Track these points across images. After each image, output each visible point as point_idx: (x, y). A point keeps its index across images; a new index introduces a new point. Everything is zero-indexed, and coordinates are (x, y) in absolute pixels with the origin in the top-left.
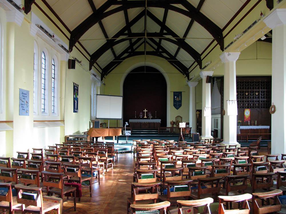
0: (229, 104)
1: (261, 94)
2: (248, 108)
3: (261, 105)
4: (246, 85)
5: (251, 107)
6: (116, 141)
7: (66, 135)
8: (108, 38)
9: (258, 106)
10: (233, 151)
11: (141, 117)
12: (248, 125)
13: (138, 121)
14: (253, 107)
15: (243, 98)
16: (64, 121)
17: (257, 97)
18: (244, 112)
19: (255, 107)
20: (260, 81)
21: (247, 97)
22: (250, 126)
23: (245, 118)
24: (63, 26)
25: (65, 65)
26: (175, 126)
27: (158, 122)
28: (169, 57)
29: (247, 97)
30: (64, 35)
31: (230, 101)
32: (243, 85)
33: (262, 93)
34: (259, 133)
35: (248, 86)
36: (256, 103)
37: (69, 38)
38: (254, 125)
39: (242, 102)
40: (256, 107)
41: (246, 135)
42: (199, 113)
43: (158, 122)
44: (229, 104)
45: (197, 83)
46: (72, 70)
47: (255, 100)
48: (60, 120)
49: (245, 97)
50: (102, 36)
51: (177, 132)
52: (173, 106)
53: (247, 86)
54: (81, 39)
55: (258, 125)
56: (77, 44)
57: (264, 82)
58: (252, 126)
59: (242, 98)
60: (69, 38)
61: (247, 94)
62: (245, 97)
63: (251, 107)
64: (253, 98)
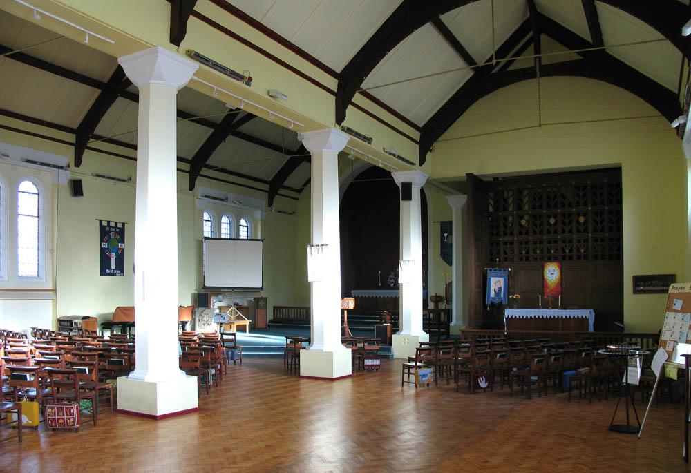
1: (562, 221)
2: (550, 259)
5: (564, 258)
7: (58, 317)
8: (476, 64)
9: (526, 255)
11: (392, 285)
12: (538, 307)
13: (376, 293)
14: (571, 258)
15: (541, 233)
16: (54, 290)
17: (582, 228)
20: (589, 182)
22: (543, 308)
23: (548, 287)
25: (66, 191)
26: (442, 306)
36: (505, 246)
38: (555, 307)
39: (538, 245)
40: (579, 258)
41: (485, 334)
46: (79, 199)
47: (575, 236)
48: (51, 288)
49: (502, 233)
50: (460, 63)
51: (299, 317)
52: (440, 257)
55: (564, 307)
57: (585, 188)
58: (548, 308)
61: (552, 221)
62: (502, 233)
63: (564, 258)
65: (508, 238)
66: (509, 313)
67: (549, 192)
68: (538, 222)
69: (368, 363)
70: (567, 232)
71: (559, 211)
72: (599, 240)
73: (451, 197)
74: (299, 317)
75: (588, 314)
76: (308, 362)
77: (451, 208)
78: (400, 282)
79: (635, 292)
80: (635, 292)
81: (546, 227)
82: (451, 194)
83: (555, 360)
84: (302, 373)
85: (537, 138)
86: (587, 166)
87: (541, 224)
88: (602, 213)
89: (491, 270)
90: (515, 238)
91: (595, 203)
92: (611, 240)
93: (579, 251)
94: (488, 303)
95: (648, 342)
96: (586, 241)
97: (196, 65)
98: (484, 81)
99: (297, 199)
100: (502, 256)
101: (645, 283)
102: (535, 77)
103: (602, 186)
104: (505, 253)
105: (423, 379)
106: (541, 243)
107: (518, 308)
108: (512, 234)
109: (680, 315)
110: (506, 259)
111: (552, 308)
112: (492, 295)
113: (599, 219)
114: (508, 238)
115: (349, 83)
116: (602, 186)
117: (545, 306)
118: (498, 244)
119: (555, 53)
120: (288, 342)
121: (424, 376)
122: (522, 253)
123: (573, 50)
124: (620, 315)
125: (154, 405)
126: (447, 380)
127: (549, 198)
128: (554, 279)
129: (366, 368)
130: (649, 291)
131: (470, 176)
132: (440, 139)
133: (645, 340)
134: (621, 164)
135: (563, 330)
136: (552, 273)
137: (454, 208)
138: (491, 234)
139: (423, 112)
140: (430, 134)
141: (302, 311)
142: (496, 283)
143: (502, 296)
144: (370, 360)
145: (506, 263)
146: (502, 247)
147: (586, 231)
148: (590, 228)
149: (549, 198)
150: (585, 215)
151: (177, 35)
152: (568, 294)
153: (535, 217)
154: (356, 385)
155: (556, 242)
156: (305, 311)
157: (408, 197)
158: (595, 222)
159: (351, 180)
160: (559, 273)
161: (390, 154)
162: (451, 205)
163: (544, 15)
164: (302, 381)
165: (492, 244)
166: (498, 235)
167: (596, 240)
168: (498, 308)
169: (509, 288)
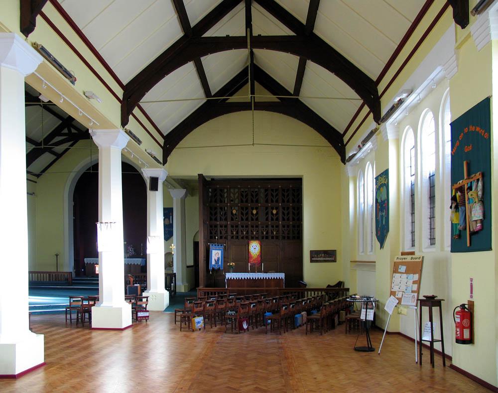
0: (101, 229)
3: (284, 233)
4: (272, 195)
6: (143, 299)
10: (300, 323)
14: (267, 238)
17: (254, 218)
18: (248, 246)
19: (270, 238)
20: (280, 187)
21: (275, 218)
23: (252, 257)
24: (395, 61)
27: (136, 264)
28: (72, 142)
29: (275, 218)
30: (111, 94)
31: (102, 224)
32: (288, 196)
33: (243, 210)
34: (244, 287)
35: (257, 197)
37: (121, 98)
38: (260, 272)
40: (272, 238)
41: (215, 291)
42: (171, 247)
43: (136, 264)
44: (101, 229)
45: (185, 192)
51: (42, 280)
53: (254, 196)
54: (144, 99)
55: (266, 272)
56: (136, 111)
57: (277, 190)
58: (255, 272)
59: (244, 220)
60: (121, 98)
64: (247, 219)
65: (224, 223)
66: (229, 276)
67: (243, 191)
68: (244, 212)
69: (140, 315)
70: (275, 219)
71: (291, 205)
72: (223, 226)
73: (175, 190)
74: (42, 280)
75: (282, 276)
76: (99, 316)
77: (172, 199)
78: (148, 252)
79: (312, 261)
80: (312, 261)
81: (250, 216)
82: (175, 187)
83: (253, 307)
84: (93, 326)
85: (247, 151)
86: (264, 176)
87: (247, 214)
88: (288, 208)
89: (212, 245)
90: (280, 223)
91: (283, 201)
92: (294, 226)
93: (272, 233)
94: (210, 268)
95: (311, 294)
96: (277, 226)
97: (40, 59)
98: (214, 106)
99: (36, 182)
100: (219, 235)
101: (316, 256)
102: (251, 109)
103: (289, 191)
104: (221, 233)
105: (198, 325)
106: (247, 226)
107: (233, 272)
108: (226, 219)
109: (405, 276)
110: (221, 237)
111: (258, 272)
112: (213, 263)
113: (286, 212)
114: (224, 223)
115: (132, 94)
116: (289, 191)
117: (253, 271)
118: (216, 226)
119: (264, 95)
120: (72, 301)
121: (199, 322)
122: (243, 234)
123: (274, 94)
124: (301, 277)
125: (13, 365)
126: (211, 325)
127: (252, 195)
128: (256, 252)
129: (139, 319)
130: (320, 260)
131: (200, 176)
132: (177, 146)
133: (309, 293)
134: (303, 176)
135: (266, 287)
136: (255, 248)
137: (174, 199)
138: (211, 219)
139: (167, 127)
140: (171, 141)
141: (45, 275)
142: (216, 254)
143: (220, 264)
144: (142, 313)
145: (221, 240)
146: (219, 228)
147: (277, 219)
148: (281, 218)
149: (252, 195)
150: (277, 209)
151: (27, 27)
152: (266, 262)
153: (242, 208)
154: (135, 332)
155: (257, 227)
156: (47, 275)
157: (154, 187)
158: (283, 213)
159: (84, 170)
160: (259, 248)
161: (149, 154)
162: (172, 196)
163: (259, 68)
164: (94, 334)
165: (211, 226)
166: (216, 220)
167: (284, 226)
168: (216, 271)
169: (225, 257)
